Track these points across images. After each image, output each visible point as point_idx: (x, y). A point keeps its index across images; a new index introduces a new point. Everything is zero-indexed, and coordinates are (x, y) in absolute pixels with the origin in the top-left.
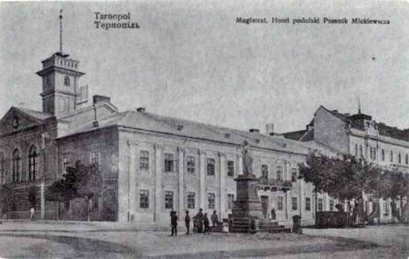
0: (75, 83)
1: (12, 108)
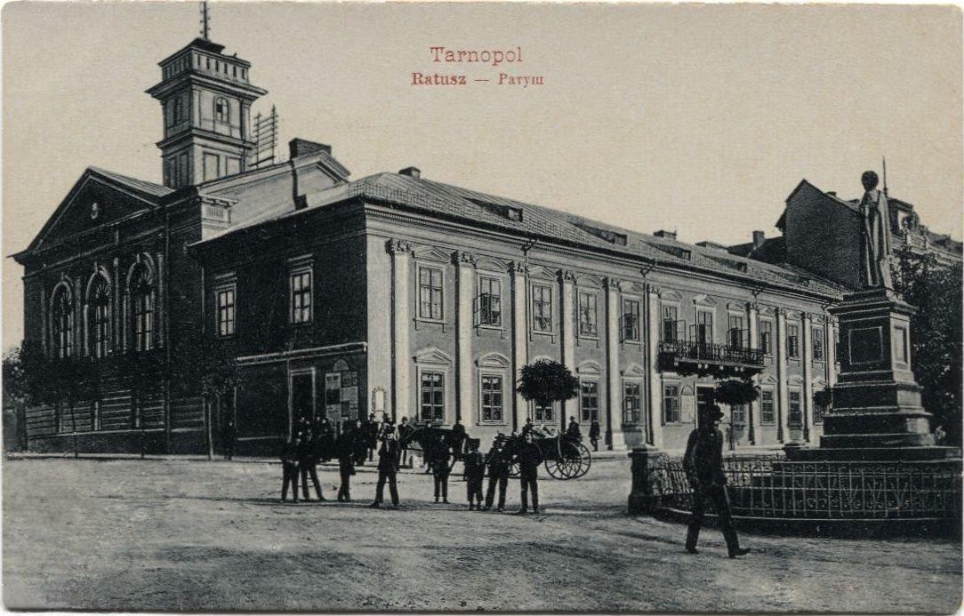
0: (242, 115)
1: (89, 171)
